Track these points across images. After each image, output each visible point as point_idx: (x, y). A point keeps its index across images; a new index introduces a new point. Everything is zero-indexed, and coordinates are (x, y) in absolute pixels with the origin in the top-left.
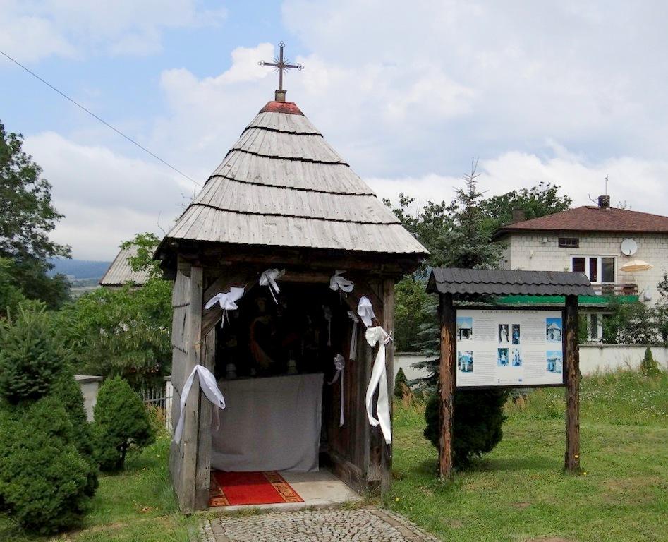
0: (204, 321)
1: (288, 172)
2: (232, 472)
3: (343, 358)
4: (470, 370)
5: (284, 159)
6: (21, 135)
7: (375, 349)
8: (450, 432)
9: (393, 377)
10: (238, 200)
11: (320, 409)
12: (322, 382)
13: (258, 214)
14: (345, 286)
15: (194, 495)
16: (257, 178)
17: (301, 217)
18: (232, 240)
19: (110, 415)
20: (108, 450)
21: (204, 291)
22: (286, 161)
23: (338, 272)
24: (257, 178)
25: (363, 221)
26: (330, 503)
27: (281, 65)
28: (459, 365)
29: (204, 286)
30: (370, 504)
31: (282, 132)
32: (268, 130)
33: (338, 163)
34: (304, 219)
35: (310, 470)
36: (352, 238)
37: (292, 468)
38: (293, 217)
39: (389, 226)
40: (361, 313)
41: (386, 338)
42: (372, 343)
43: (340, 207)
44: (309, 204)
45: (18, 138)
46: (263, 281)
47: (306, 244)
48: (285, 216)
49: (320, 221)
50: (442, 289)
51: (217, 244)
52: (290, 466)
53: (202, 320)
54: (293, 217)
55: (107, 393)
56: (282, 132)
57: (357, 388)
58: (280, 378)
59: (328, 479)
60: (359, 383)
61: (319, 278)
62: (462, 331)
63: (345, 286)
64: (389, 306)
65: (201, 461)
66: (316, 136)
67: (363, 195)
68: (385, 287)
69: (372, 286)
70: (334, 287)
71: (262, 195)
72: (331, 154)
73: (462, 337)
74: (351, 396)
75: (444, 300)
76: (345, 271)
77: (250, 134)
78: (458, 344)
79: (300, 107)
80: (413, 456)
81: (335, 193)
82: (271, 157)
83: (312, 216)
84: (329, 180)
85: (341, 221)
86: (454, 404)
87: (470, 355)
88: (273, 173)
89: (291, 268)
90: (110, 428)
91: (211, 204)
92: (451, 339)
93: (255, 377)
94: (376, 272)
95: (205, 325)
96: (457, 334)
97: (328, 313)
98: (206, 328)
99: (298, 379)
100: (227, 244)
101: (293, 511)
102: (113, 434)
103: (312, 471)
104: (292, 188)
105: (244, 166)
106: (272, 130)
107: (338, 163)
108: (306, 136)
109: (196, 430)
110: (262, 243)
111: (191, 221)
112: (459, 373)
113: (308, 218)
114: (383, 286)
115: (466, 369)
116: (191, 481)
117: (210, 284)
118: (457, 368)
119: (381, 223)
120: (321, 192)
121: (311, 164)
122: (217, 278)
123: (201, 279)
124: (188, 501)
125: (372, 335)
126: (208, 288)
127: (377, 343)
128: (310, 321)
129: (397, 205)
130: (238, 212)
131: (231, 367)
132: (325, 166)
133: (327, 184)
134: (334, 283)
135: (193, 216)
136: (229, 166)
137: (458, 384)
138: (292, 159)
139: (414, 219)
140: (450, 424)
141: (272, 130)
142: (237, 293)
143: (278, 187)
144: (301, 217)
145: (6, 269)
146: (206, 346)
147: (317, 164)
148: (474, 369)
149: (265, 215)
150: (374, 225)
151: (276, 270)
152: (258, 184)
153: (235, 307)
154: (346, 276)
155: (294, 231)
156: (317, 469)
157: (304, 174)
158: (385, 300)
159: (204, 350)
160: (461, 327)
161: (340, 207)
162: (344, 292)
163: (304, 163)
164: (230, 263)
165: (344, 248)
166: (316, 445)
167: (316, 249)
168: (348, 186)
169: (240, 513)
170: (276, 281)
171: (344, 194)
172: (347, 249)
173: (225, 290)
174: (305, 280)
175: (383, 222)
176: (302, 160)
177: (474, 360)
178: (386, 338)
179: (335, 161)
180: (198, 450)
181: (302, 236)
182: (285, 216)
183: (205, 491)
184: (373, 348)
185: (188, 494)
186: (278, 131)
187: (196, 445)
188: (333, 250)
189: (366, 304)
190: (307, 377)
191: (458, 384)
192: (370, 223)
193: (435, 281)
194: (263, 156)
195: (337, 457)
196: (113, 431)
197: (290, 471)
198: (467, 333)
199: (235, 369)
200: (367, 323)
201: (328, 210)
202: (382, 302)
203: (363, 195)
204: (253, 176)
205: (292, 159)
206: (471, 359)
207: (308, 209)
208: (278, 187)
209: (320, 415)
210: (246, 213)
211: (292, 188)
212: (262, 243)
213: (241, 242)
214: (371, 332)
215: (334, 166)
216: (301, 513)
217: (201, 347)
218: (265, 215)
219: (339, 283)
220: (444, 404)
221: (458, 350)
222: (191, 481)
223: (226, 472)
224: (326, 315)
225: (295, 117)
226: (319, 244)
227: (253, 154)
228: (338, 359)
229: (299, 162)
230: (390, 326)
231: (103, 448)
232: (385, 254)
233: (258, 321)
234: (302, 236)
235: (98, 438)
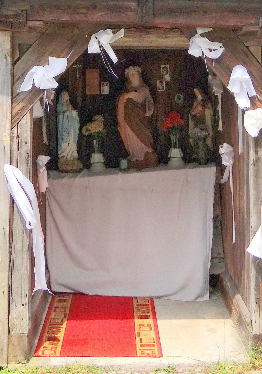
3: (231, 149)
14: (211, 50)
23: (200, 31)
35: (196, 298)
37: (169, 295)
52: (169, 293)
53: (12, 103)
58: (158, 172)
59: (215, 317)
60: (245, 185)
63: (211, 50)
69: (252, 49)
70: (194, 52)
74: (240, 203)
76: (211, 29)
93: (125, 171)
94: (252, 28)
95: (15, 111)
97: (216, 86)
103: (200, 299)
126: (19, 59)
146: (18, 137)
148: (163, 355)
154: (211, 37)
156: (207, 297)
162: (210, 60)
164: (40, 24)
173: (41, 61)
195: (229, 284)
209: (210, 224)
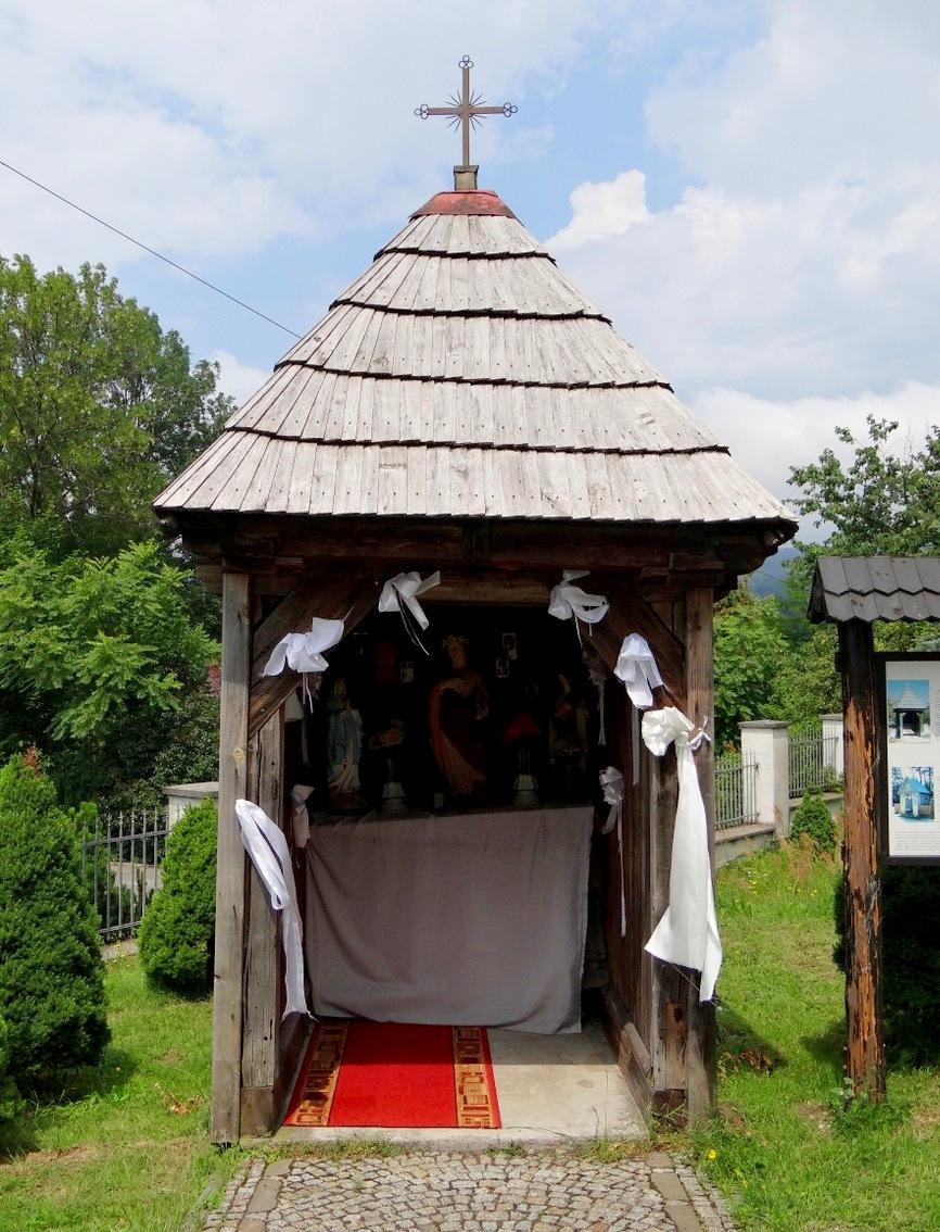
0: (253, 699)
1: (455, 342)
2: (391, 1024)
4: (927, 815)
5: (449, 314)
6: (217, 365)
7: (669, 762)
8: (873, 973)
9: (658, 843)
10: (327, 413)
11: (584, 887)
12: (589, 829)
13: (367, 444)
14: (586, 608)
15: (236, 1099)
16: (378, 361)
17: (469, 446)
18: (297, 507)
19: (186, 879)
20: (183, 949)
21: (253, 628)
22: (452, 320)
23: (568, 576)
24: (378, 361)
25: (624, 448)
26: (558, 1137)
27: (466, 111)
28: (897, 801)
29: (251, 616)
30: (658, 1148)
31: (455, 256)
32: (422, 253)
33: (579, 315)
34: (477, 452)
35: (559, 1029)
36: (592, 491)
38: (452, 446)
39: (694, 457)
40: (623, 674)
41: (692, 735)
42: (657, 748)
43: (571, 417)
44: (450, 413)
45: (213, 369)
46: (388, 603)
47: (473, 509)
48: (430, 445)
49: (517, 454)
50: (840, 609)
51: (259, 518)
52: (514, 1019)
53: (250, 695)
54: (452, 446)
55: (184, 834)
56: (455, 256)
57: (640, 849)
61: (523, 593)
62: (902, 715)
63: (586, 608)
64: (700, 656)
65: (251, 1022)
66: (534, 260)
67: (634, 385)
68: (690, 609)
69: (656, 607)
70: (559, 611)
71: (384, 399)
72: (565, 296)
73: (903, 731)
75: (851, 637)
77: (386, 270)
78: (894, 749)
79: (506, 200)
80: (823, 999)
81: (563, 386)
82: (418, 313)
83: (497, 443)
84: (552, 356)
85: (569, 450)
86: (881, 901)
87: (925, 778)
88: (414, 345)
89: (456, 571)
90: (185, 905)
91: (260, 427)
92: (869, 738)
94: (656, 572)
95: (255, 709)
96: (890, 722)
98: (259, 713)
99: (536, 815)
100: (282, 518)
101: (467, 1153)
102: (192, 918)
104: (459, 380)
105: (354, 338)
106: (431, 254)
107: (579, 315)
108: (510, 262)
109: (240, 950)
110: (363, 511)
111: (210, 466)
112: (896, 823)
113: (486, 447)
114: (685, 608)
115: (916, 812)
116: (229, 1067)
117: (266, 614)
118: (891, 809)
119: (672, 451)
120: (528, 385)
121: (512, 322)
122: (281, 598)
123: (245, 600)
124: (223, 1112)
125: (657, 729)
127: (672, 748)
128: (567, 688)
129: (864, 439)
130: (320, 442)
131: (393, 789)
132: (547, 325)
133: (545, 367)
134: (557, 601)
135: (216, 456)
136: (317, 340)
137: (896, 850)
138: (467, 314)
139: (903, 464)
140: (872, 953)
141: (431, 254)
142: (328, 632)
143: (425, 379)
144: (469, 446)
145: (177, 590)
146: (259, 753)
147: (527, 322)
149: (383, 444)
150: (654, 457)
151: (415, 575)
152: (379, 376)
153: (324, 665)
154: (589, 586)
155: (447, 478)
156: (577, 1028)
157: (493, 346)
158: (689, 640)
159: (254, 764)
160: (901, 706)
161: (571, 417)
162: (584, 625)
163: (496, 321)
164: (299, 561)
165: (569, 515)
166: (574, 971)
167: (497, 520)
168: (595, 369)
169: (341, 1148)
170: (424, 603)
171: (586, 385)
172: (576, 516)
173: (301, 625)
174: (490, 598)
175: (677, 448)
176: (491, 314)
177: (935, 790)
178: (692, 735)
179: (573, 310)
180: (245, 993)
181: (465, 492)
182: (430, 445)
183: (261, 1093)
184: (661, 759)
185: (224, 1096)
186: (443, 255)
187: (239, 985)
188: (540, 521)
189: (636, 653)
190: (553, 816)
191: (896, 850)
192: (644, 452)
193: (824, 591)
194: (401, 312)
196: (191, 911)
197: (512, 1028)
198: (913, 720)
199: (402, 794)
200: (639, 697)
201: (539, 425)
202: (684, 648)
203: (634, 385)
204: (368, 358)
205: (467, 314)
206: (929, 786)
207: (490, 426)
208: (425, 379)
209: (584, 902)
210: (339, 443)
211: (459, 380)
212: (364, 509)
213: (315, 510)
214: (654, 722)
215: (569, 323)
216: (485, 1159)
217: (249, 756)
218: (383, 444)
219: (571, 604)
220: (856, 902)
221: (893, 761)
222: (229, 1067)
223: (377, 1022)
224: (593, 675)
225: (488, 222)
226: (503, 509)
227: (377, 308)
228: (608, 777)
229: (485, 320)
230: (704, 707)
231: (173, 946)
232: (674, 525)
233: (449, 692)
234: (465, 492)
235: (164, 924)
